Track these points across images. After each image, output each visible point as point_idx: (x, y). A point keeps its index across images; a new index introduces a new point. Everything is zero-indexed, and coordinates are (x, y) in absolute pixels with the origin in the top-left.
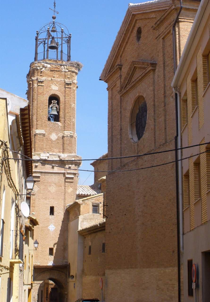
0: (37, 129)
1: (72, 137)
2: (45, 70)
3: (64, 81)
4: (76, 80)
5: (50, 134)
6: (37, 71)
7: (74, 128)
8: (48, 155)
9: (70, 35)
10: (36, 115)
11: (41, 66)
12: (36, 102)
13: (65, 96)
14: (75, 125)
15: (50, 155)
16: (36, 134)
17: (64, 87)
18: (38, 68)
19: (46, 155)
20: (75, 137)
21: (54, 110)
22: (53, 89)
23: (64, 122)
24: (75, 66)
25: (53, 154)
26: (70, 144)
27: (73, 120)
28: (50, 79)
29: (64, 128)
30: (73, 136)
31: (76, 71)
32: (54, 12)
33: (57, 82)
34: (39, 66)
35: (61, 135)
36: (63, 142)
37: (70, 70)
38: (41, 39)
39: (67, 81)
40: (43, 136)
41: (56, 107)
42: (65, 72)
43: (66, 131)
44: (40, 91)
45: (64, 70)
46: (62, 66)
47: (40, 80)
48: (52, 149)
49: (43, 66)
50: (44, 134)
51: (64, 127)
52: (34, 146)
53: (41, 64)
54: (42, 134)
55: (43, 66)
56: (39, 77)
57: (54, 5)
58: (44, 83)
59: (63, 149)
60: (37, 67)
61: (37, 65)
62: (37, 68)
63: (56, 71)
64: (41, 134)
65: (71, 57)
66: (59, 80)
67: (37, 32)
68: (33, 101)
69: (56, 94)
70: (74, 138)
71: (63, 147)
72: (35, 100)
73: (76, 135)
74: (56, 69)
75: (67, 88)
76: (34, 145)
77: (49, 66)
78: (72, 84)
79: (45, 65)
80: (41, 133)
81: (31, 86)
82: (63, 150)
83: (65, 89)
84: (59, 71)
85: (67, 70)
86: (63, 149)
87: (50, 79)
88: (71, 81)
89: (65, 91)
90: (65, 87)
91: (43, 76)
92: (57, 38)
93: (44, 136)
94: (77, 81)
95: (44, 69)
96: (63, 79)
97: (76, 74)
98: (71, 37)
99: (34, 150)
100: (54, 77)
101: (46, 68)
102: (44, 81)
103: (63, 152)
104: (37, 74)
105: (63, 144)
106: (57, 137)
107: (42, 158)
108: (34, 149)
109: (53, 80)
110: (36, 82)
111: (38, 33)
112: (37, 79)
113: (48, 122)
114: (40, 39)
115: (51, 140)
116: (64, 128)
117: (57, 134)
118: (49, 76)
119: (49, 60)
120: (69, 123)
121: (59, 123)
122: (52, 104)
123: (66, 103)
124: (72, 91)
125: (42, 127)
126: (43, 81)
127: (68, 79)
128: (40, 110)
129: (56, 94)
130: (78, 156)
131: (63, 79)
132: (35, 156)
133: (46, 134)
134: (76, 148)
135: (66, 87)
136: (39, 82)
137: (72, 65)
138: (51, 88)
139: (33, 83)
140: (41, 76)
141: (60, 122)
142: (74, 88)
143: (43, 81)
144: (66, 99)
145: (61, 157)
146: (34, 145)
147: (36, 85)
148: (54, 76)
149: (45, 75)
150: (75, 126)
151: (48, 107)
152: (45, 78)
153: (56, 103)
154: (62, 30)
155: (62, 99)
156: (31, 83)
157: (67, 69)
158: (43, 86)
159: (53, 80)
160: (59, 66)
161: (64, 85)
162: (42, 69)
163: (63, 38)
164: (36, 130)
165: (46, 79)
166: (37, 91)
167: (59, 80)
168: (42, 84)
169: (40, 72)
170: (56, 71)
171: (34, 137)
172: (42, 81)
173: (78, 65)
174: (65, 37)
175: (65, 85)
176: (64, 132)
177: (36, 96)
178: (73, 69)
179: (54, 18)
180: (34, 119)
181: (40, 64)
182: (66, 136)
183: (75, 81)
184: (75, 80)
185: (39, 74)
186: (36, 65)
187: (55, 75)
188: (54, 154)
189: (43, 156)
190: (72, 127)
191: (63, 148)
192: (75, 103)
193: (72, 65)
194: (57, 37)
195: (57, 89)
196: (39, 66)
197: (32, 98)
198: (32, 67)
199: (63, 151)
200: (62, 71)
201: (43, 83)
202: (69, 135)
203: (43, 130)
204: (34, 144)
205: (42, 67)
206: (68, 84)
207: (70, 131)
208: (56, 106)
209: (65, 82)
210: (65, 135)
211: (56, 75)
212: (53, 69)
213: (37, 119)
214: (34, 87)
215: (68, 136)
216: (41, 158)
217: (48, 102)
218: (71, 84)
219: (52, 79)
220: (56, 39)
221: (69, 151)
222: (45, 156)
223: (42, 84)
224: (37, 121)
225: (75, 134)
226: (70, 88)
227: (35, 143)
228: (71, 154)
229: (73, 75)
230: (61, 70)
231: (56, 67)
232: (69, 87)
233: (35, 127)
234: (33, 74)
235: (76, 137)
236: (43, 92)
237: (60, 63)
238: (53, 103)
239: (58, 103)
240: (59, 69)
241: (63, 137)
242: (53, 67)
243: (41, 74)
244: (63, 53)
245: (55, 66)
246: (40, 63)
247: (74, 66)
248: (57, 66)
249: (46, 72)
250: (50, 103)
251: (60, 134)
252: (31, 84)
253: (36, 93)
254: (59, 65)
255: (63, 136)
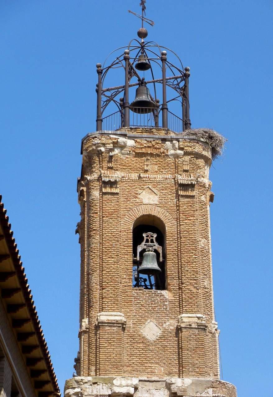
0: (102, 309)
1: (204, 329)
2: (119, 155)
3: (175, 181)
4: (208, 177)
5: (141, 321)
6: (98, 157)
7: (207, 307)
8: (135, 381)
9: (187, 70)
10: (98, 271)
11: (109, 144)
12: (98, 236)
13: (178, 219)
14: (212, 297)
15: (140, 381)
16: (99, 323)
17: (175, 195)
18: (103, 149)
19: (129, 382)
20: (213, 330)
21: (149, 259)
22: (145, 201)
23: (180, 288)
24: (202, 139)
25: (150, 379)
26: (200, 346)
27: (205, 284)
28: (134, 176)
29: (180, 306)
30: (206, 327)
31: (205, 153)
32: (143, 20)
33: (156, 183)
34: (104, 145)
35: (171, 325)
36: (178, 346)
37: (189, 149)
38: (112, 89)
39: (183, 179)
40: (121, 328)
41: (156, 251)
42: (176, 156)
43: (187, 312)
44: (109, 207)
45: (172, 152)
46: (168, 143)
47: (107, 180)
48: (146, 365)
49: (113, 143)
50: (123, 324)
51: (181, 301)
52: (96, 357)
53: (110, 138)
54: (117, 322)
55: (116, 144)
56: (106, 171)
57: (141, 4)
58: (118, 186)
59: (181, 365)
60: (97, 145)
61: (99, 141)
62: (99, 149)
63: (151, 155)
64: (114, 323)
65: (190, 124)
66: (159, 177)
67: (98, 66)
68: (89, 236)
69: (154, 216)
70: (211, 333)
71: (179, 358)
72: (94, 232)
73: (216, 326)
74: (150, 149)
75: (182, 196)
76: (96, 355)
77: (130, 143)
78: (196, 186)
79: (121, 140)
80: (114, 322)
81: (85, 199)
82: (179, 368)
83: (179, 200)
84: (158, 156)
85: (181, 152)
86: (179, 363)
87: (134, 176)
88: (192, 178)
89: (177, 206)
90: (178, 196)
91: (117, 170)
92: (154, 82)
93: (124, 329)
94: (210, 179)
95: (117, 151)
96: (170, 176)
97: (207, 161)
98: (189, 75)
99: (96, 370)
100: (146, 171)
101: (122, 147)
102: (118, 180)
103: (180, 374)
104: (99, 166)
105: (179, 350)
106: (160, 332)
107: (117, 390)
108: (96, 368)
109: (144, 179)
110: (97, 184)
111: (102, 70)
112: (99, 178)
113: (135, 292)
114: (108, 90)
115: (144, 340)
116: (180, 306)
117: (160, 324)
118: (133, 169)
119: (131, 129)
120: (194, 290)
121: (164, 292)
122: (144, 243)
123: (181, 238)
124: (197, 206)
125: (116, 306)
126: (116, 181)
127: (184, 174)
128: (109, 257)
129: (153, 214)
130: (223, 384)
131: (170, 175)
132: (96, 385)
133: (130, 324)
134: (216, 363)
135: (179, 195)
136: (106, 184)
137: (194, 137)
138: (138, 200)
139: (89, 189)
140: (111, 168)
141: (166, 291)
142: (203, 198)
143: (116, 181)
144: (180, 225)
145: (173, 387)
146: (96, 355)
147: (96, 194)
148: (146, 168)
149: (121, 167)
150: (213, 301)
151: (131, 250)
152: (123, 174)
153: (154, 240)
154: (163, 54)
155: (170, 228)
156: (83, 190)
157: (181, 149)
158: (117, 194)
159: (144, 179)
160: (158, 143)
161: (174, 191)
162: (111, 150)
163: (168, 81)
164: (99, 314)
165: (123, 177)
166: (102, 208)
167: (159, 177)
168: (114, 190)
169: (107, 159)
170: (151, 155)
171: (96, 334)
172: (112, 180)
173: (211, 137)
174: (173, 78)
175: (177, 191)
176: (179, 317)
177: (98, 223)
178: (198, 149)
179: (142, 35)
180: (94, 285)
181: (107, 139)
182: (185, 328)
183: (206, 181)
184: (203, 177)
185: (105, 164)
186: (97, 141)
187: (147, 165)
188: (154, 378)
189: (120, 386)
190: (201, 301)
191: (179, 361)
192: (206, 238)
193: (194, 137)
194: (152, 80)
195: (157, 203)
196: (104, 145)
197: (89, 228)
198: (86, 150)
199: (179, 371)
200: (167, 155)
201: (116, 188)
202: (194, 323)
203: (120, 312)
204: (96, 354)
205: (112, 145)
206: (185, 187)
207: (198, 312)
208: (154, 248)
209: (176, 183)
210: (183, 325)
211: (152, 165)
212: (144, 151)
213: (101, 282)
214: (92, 199)
215: (193, 326)
216: (115, 393)
217: (131, 236)
218: (192, 186)
219: (140, 177)
220: (150, 86)
221: (198, 370)
222: (127, 386)
223: (114, 190)
224: (103, 289)
225: (213, 322)
226: (193, 197)
227: (96, 349)
228: (202, 379)
229: (197, 163)
230: (164, 153)
231: (150, 145)
232: (189, 193)
233: (97, 306)
234: (90, 168)
235: (216, 330)
236: (116, 211)
237: (162, 134)
238: (147, 241)
239: (161, 240)
240: (160, 149)
241: (179, 330)
242: (141, 144)
243: (110, 165)
244: (169, 114)
245: (148, 142)
246: (106, 136)
247: (198, 141)
248: (153, 143)
249: (124, 158)
250: (137, 239)
251: (167, 323)
252: (85, 193)
253: (96, 213)
254: (158, 139)
255: (177, 328)
